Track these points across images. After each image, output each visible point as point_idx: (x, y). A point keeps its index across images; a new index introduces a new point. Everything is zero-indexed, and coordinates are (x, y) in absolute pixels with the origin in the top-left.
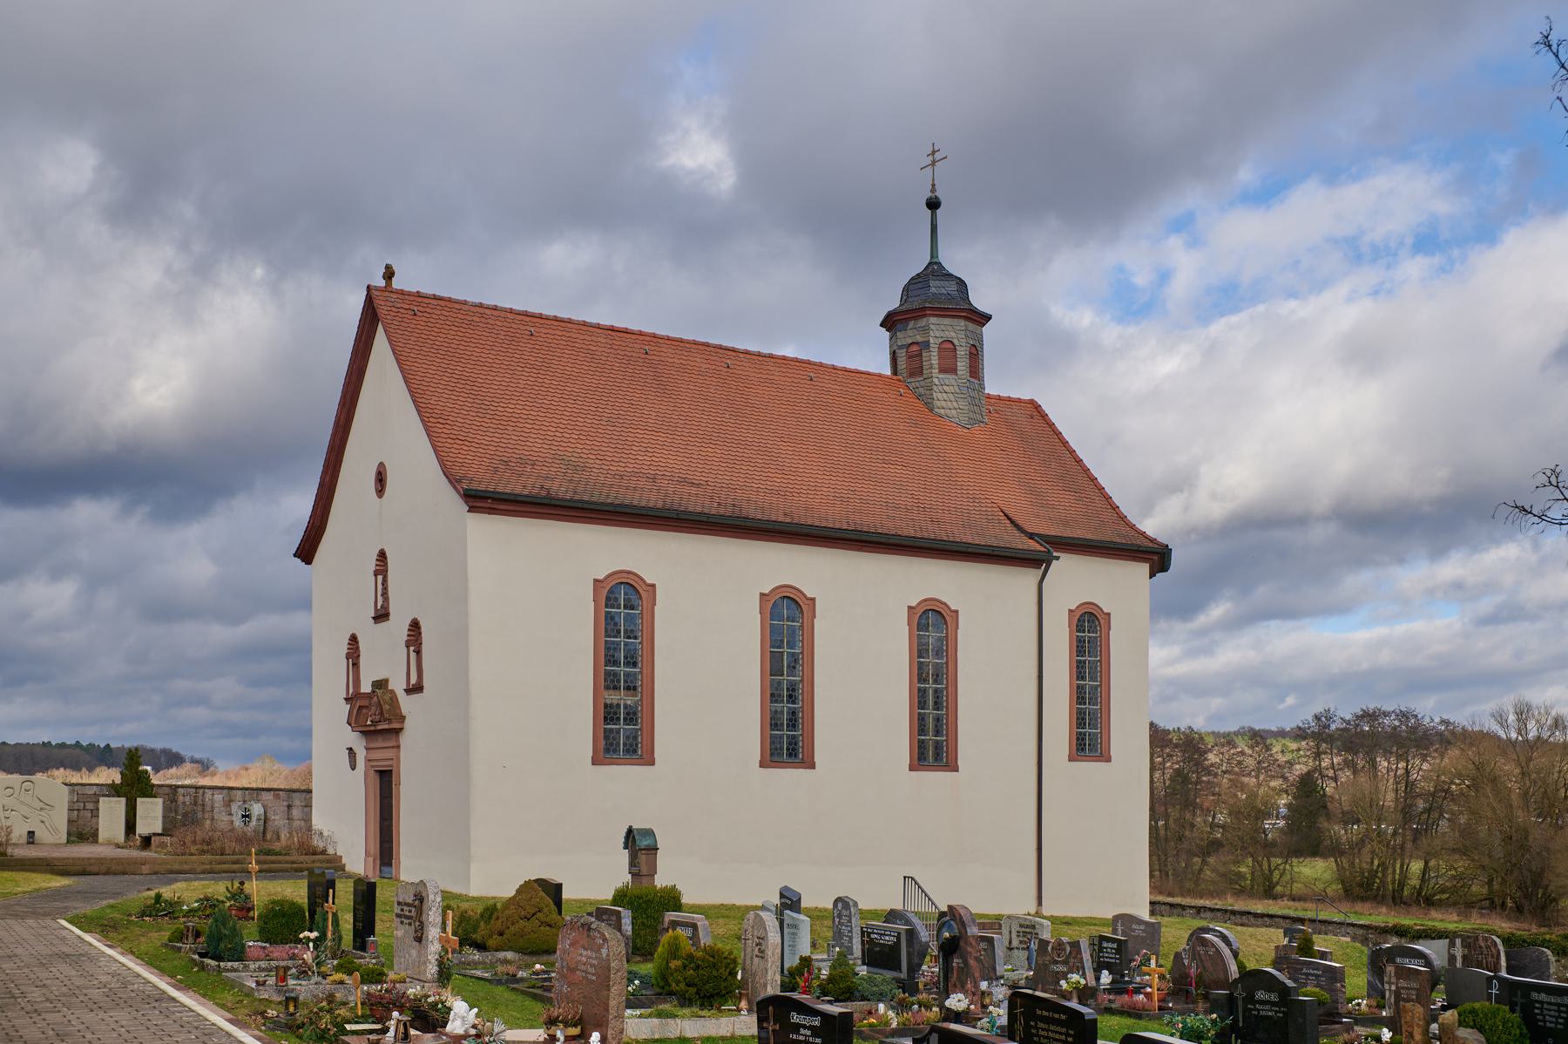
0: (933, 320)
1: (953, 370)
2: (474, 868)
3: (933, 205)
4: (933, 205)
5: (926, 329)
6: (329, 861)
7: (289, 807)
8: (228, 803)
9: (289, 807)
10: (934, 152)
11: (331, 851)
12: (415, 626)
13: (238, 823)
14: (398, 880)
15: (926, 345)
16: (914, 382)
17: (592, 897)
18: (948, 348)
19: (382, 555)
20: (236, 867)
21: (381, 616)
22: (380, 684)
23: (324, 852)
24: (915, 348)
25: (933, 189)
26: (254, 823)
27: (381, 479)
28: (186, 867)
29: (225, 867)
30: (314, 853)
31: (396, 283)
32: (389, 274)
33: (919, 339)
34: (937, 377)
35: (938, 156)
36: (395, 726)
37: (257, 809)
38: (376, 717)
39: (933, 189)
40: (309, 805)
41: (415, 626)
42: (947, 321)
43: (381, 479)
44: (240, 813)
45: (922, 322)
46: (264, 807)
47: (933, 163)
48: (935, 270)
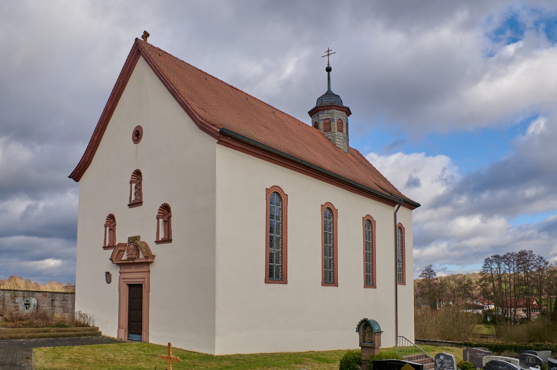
0: (335, 111)
1: (342, 131)
2: (218, 340)
3: (329, 70)
4: (329, 70)
5: (332, 114)
6: (92, 330)
7: (53, 300)
8: (14, 298)
9: (53, 300)
10: (328, 51)
11: (91, 325)
12: (166, 209)
13: (21, 307)
14: (148, 343)
15: (333, 120)
16: (327, 134)
17: (254, 353)
18: (340, 123)
19: (138, 173)
20: (46, 334)
21: (136, 203)
22: (134, 240)
23: (87, 325)
24: (328, 121)
25: (329, 65)
26: (32, 308)
27: (138, 135)
28: (19, 335)
29: (41, 334)
30: (83, 326)
31: (150, 40)
32: (146, 35)
33: (329, 117)
34: (337, 133)
35: (330, 52)
36: (150, 260)
37: (33, 301)
38: (132, 258)
39: (329, 65)
40: (74, 299)
41: (166, 209)
42: (340, 112)
43: (138, 135)
44: (23, 303)
45: (331, 111)
46: (37, 300)
47: (328, 55)
48: (329, 93)
